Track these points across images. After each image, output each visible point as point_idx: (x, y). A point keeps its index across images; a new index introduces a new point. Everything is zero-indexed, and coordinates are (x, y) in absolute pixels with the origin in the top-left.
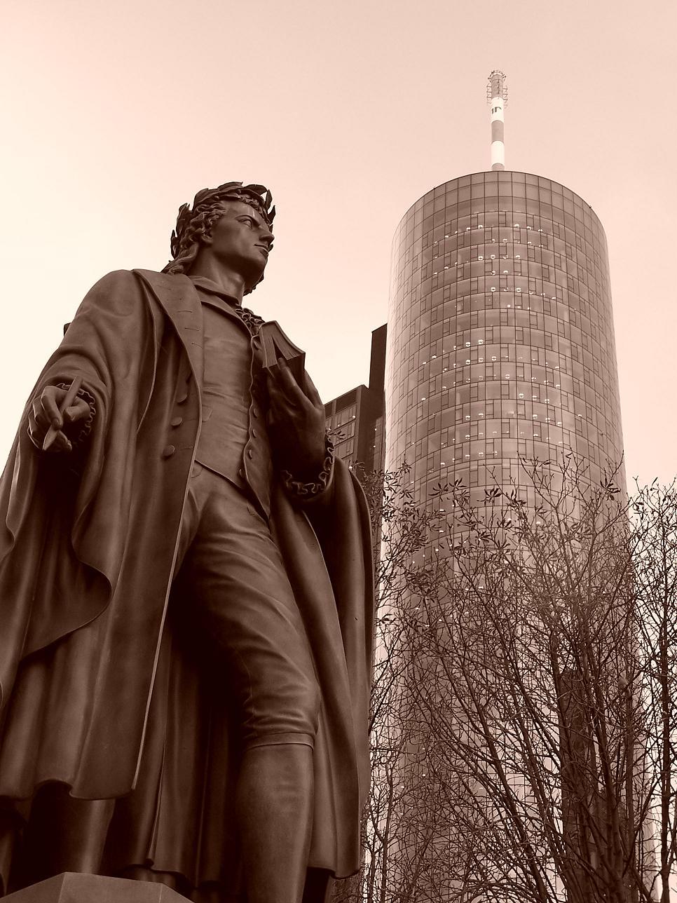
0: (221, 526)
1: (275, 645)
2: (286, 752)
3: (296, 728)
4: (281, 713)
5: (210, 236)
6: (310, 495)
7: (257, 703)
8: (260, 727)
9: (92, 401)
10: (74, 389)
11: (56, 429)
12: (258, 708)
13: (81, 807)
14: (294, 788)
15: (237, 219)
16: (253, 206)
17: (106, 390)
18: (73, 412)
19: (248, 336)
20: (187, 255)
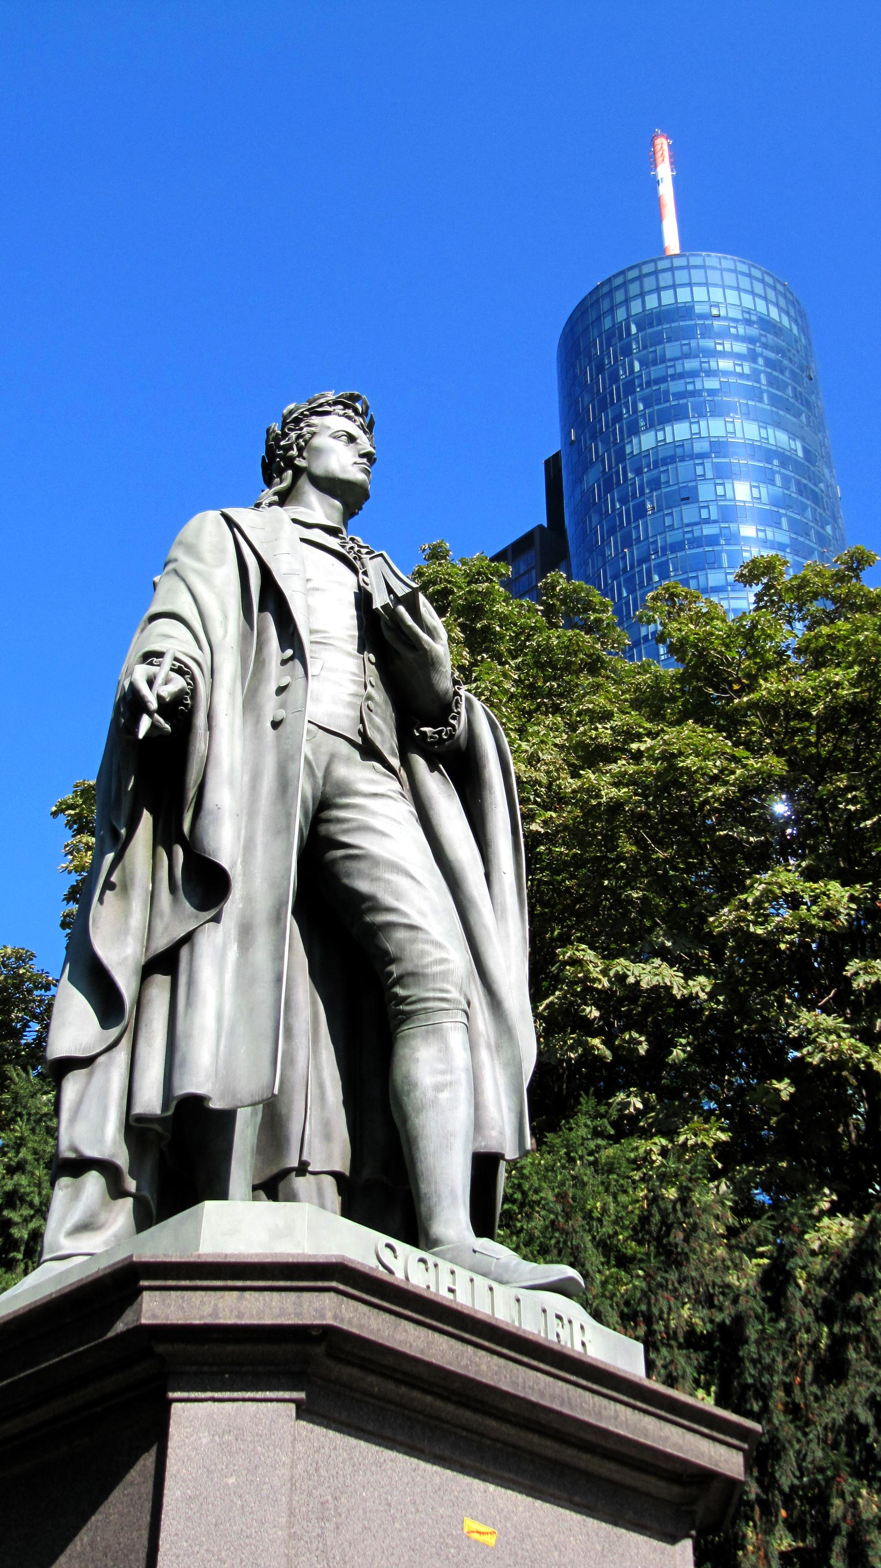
0: (345, 790)
1: (416, 919)
2: (436, 1031)
3: (444, 1005)
4: (427, 990)
5: (304, 458)
6: (441, 741)
7: (400, 980)
8: (408, 1008)
9: (188, 673)
10: (167, 662)
11: (150, 714)
12: (403, 987)
13: (227, 1117)
14: (450, 1071)
15: (330, 436)
16: (349, 418)
17: (204, 658)
18: (167, 692)
19: (355, 570)
20: (281, 482)
